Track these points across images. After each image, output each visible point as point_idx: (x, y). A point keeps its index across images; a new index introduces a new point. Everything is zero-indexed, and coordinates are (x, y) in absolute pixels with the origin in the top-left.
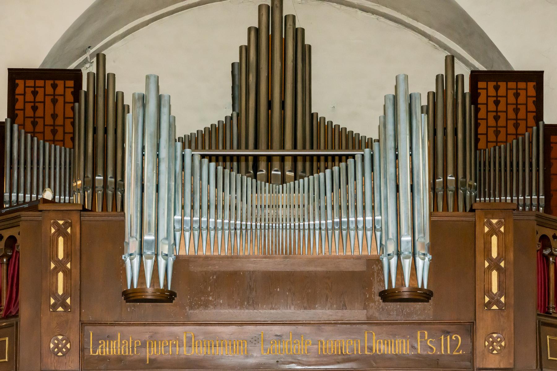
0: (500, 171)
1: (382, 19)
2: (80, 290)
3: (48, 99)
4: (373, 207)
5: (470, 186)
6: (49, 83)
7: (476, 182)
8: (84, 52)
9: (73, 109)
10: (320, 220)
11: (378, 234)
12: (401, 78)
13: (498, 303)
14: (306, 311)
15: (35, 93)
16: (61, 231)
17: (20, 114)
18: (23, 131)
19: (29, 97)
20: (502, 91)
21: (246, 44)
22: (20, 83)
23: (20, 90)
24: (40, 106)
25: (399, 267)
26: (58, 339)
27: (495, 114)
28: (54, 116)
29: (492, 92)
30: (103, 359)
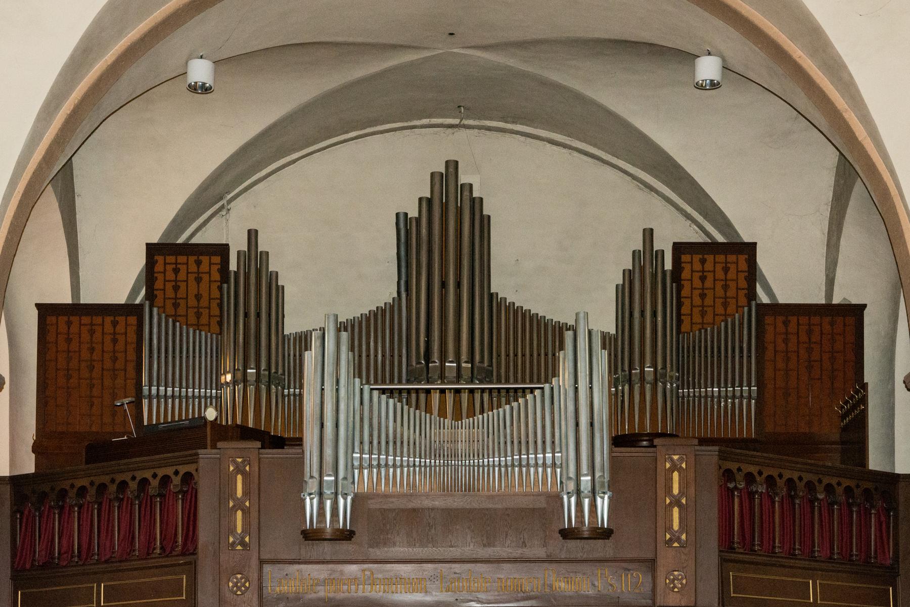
0: (706, 357)
1: (576, 154)
2: (257, 527)
3: (192, 277)
4: (553, 442)
5: (671, 377)
6: (192, 259)
7: (678, 372)
8: (221, 198)
9: (220, 289)
10: (499, 457)
11: (558, 470)
12: (582, 315)
13: (678, 540)
14: (486, 549)
15: (176, 271)
16: (239, 470)
17: (159, 294)
18: (163, 316)
19: (170, 275)
20: (709, 266)
21: (417, 215)
22: (160, 259)
23: (159, 267)
24: (183, 286)
25: (579, 505)
26: (237, 578)
27: (700, 291)
28: (198, 297)
29: (697, 266)
30: (282, 598)
